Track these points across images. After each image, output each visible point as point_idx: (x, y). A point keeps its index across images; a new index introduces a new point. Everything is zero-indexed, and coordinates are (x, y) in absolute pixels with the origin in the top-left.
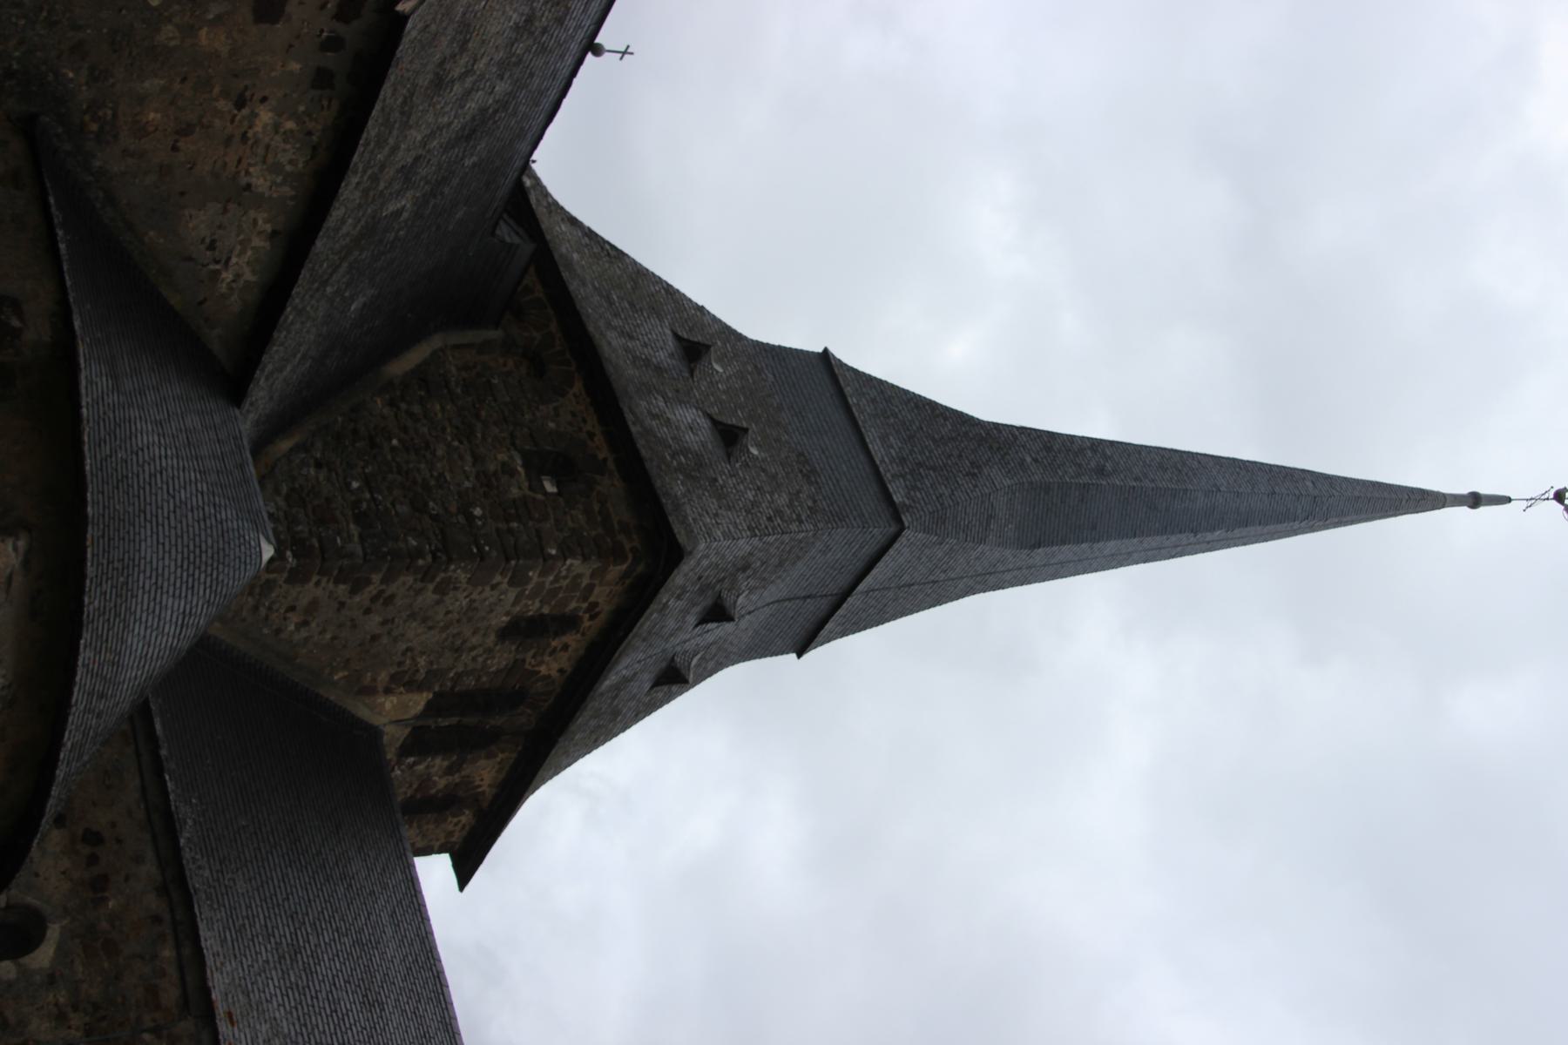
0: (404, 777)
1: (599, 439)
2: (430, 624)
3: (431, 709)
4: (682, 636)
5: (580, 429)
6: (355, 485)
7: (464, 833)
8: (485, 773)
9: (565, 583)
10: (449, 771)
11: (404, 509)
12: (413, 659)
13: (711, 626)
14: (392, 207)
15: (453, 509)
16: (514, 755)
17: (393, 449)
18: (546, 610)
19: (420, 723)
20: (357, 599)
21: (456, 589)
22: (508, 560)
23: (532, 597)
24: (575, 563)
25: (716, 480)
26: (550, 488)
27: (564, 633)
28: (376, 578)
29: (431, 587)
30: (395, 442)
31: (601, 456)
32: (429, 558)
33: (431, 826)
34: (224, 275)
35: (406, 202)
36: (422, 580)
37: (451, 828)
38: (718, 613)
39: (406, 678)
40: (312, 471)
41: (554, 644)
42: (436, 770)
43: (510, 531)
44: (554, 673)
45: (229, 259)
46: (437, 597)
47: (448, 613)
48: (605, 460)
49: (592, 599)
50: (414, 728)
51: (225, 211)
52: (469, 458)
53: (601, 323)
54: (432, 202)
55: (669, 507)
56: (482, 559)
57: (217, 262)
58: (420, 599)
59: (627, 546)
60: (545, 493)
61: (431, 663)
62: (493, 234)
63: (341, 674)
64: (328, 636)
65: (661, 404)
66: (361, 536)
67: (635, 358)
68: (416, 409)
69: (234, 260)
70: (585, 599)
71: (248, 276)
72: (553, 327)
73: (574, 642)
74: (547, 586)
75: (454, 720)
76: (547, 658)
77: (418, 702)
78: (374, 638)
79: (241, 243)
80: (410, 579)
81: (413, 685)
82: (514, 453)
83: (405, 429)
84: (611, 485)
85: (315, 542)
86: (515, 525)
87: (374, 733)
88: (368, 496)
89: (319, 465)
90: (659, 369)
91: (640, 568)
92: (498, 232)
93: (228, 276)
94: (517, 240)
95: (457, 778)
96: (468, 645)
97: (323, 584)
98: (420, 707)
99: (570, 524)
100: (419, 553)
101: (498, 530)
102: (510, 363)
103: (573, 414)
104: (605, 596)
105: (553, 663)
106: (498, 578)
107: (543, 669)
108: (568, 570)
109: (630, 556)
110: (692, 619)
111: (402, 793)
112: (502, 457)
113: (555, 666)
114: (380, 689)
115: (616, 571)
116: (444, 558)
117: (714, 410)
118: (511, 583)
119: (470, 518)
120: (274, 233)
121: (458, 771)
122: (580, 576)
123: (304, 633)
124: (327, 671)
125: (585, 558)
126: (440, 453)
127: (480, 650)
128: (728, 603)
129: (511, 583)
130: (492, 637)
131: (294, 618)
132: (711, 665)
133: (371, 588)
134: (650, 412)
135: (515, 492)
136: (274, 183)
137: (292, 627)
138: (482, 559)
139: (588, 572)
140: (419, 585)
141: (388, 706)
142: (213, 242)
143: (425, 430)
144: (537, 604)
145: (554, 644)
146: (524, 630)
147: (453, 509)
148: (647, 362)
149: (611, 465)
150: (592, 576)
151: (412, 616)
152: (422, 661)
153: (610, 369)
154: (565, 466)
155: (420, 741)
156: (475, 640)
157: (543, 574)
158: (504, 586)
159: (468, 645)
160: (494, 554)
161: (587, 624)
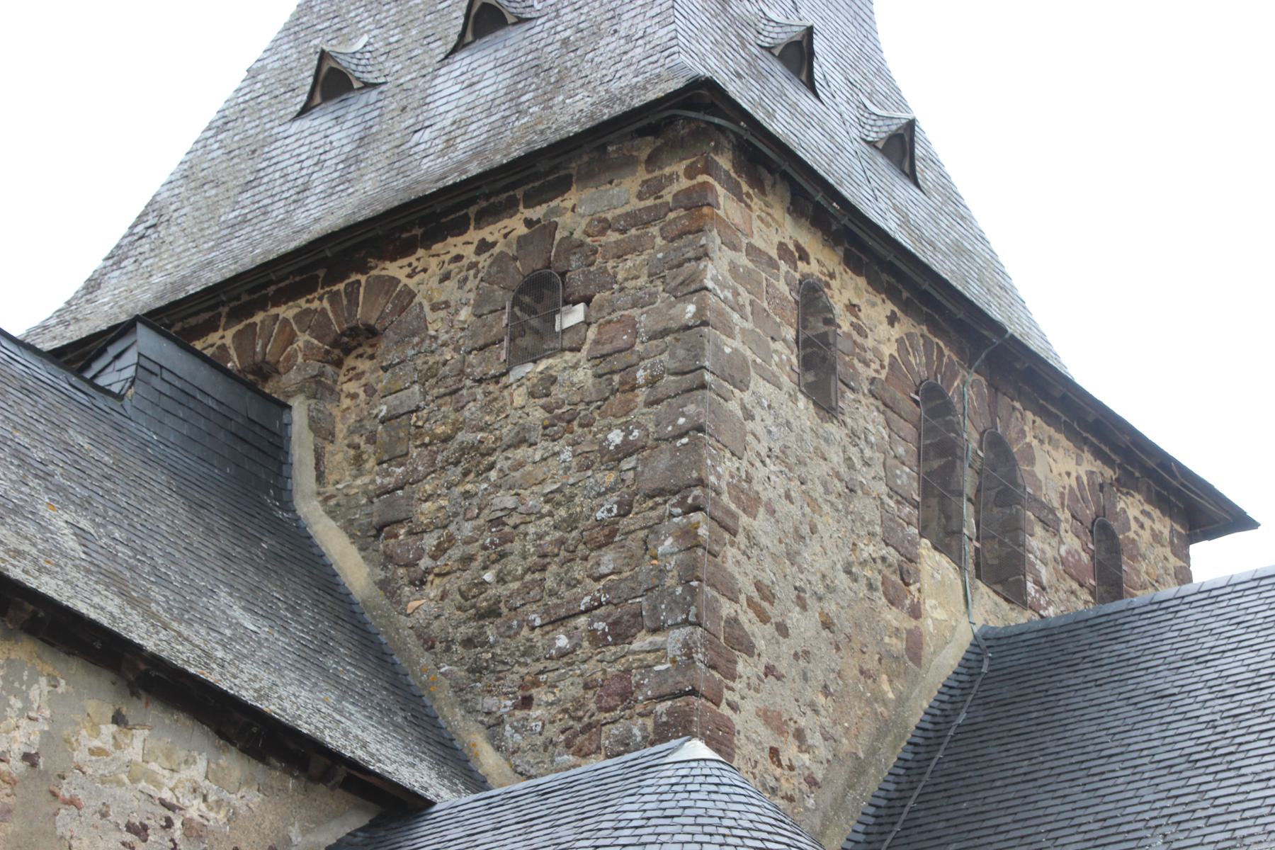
0: (1058, 597)
1: (491, 232)
2: (805, 530)
3: (947, 542)
4: (833, 123)
5: (473, 265)
6: (562, 641)
7: (1156, 513)
8: (1057, 467)
9: (745, 298)
10: (1050, 525)
11: (608, 560)
12: (863, 563)
13: (818, 75)
14: (70, 543)
15: (610, 478)
16: (1029, 415)
17: (501, 579)
18: (790, 334)
19: (971, 567)
20: (761, 644)
21: (749, 480)
22: (703, 386)
23: (767, 355)
24: (714, 272)
25: (565, 42)
26: (575, 315)
27: (829, 309)
28: (727, 609)
29: (744, 519)
30: (488, 576)
31: (522, 230)
32: (696, 517)
33: (1143, 567)
34: (193, 813)
35: (60, 520)
36: (734, 534)
37: (1146, 535)
38: (798, 56)
39: (896, 578)
40: (536, 712)
41: (846, 327)
42: (1052, 550)
43: (652, 382)
44: (896, 332)
45: (163, 803)
46: (762, 510)
47: (788, 497)
48: (529, 223)
49: (774, 253)
50: (978, 577)
51: (72, 802)
52: (520, 453)
53: (281, 233)
54: (58, 479)
55: (618, 109)
56: (700, 429)
57: (169, 823)
58: (764, 540)
59: (685, 183)
60: (587, 323)
61: (872, 535)
62: (119, 397)
63: (886, 687)
64: (821, 700)
65: (427, 134)
66: (654, 631)
67: (345, 180)
68: (430, 541)
69: (167, 795)
70: (772, 264)
71: (197, 771)
72: (287, 312)
73: (846, 290)
74: (749, 325)
75: (968, 509)
76: (869, 343)
77: (935, 567)
78: (827, 625)
79: (134, 780)
80: (731, 553)
81: (906, 572)
82: (512, 377)
83: (467, 560)
84: (575, 211)
85: (662, 707)
86: (641, 375)
87: (987, 645)
88: (582, 621)
89: (527, 702)
90: (362, 141)
91: (724, 162)
92: (116, 389)
93: (195, 809)
94: (131, 358)
95: (1064, 515)
96: (843, 469)
97: (735, 697)
98: (943, 560)
99: (642, 281)
100: (689, 539)
101: (649, 404)
102: (352, 387)
103: (446, 277)
104: (767, 225)
105: (876, 330)
106: (733, 406)
107: (889, 350)
108: (723, 286)
109: (701, 178)
110: (806, 102)
111: (1082, 603)
112: (519, 397)
113: (883, 329)
114: (911, 624)
115: (727, 206)
116: (697, 491)
117: (440, 49)
118: (742, 385)
119: (627, 450)
120: (118, 719)
121: (1052, 511)
122: (733, 268)
123: (815, 739)
124: (880, 709)
125: (704, 254)
126: (510, 502)
127: (853, 452)
128: (783, 37)
129: (742, 385)
130: (832, 428)
131: (790, 751)
132: (880, 86)
133: (743, 619)
134: (443, 153)
135: (584, 375)
136: (22, 713)
137: (806, 757)
138: (700, 429)
139: (729, 254)
140: (741, 538)
141: (940, 614)
142: (130, 828)
143: (468, 526)
144: (779, 346)
145: (846, 327)
146: (819, 367)
147: (610, 478)
148: (352, 160)
149: (537, 213)
150: (734, 247)
151: (792, 556)
152: (869, 550)
153: (367, 213)
154: (538, 291)
155: (1003, 571)
156: (836, 457)
157: (729, 331)
158: (747, 397)
159: (843, 469)
160: (691, 408)
161: (813, 268)
